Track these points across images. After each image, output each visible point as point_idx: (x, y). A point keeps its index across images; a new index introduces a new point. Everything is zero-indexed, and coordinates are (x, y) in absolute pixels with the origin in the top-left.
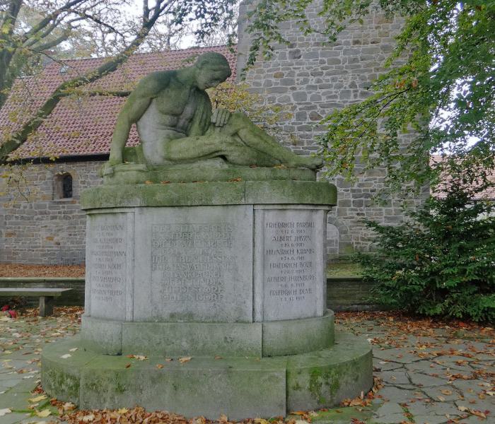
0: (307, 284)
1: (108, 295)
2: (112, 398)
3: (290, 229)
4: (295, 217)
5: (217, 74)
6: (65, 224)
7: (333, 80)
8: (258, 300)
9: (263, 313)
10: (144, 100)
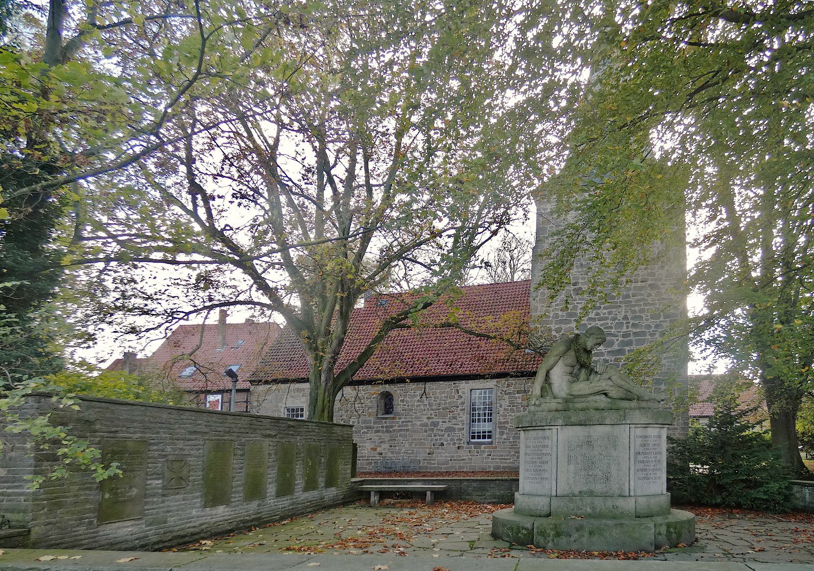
1: (539, 480)
2: (553, 540)
5: (599, 341)
6: (386, 437)
7: (609, 313)
8: (632, 483)
9: (635, 490)
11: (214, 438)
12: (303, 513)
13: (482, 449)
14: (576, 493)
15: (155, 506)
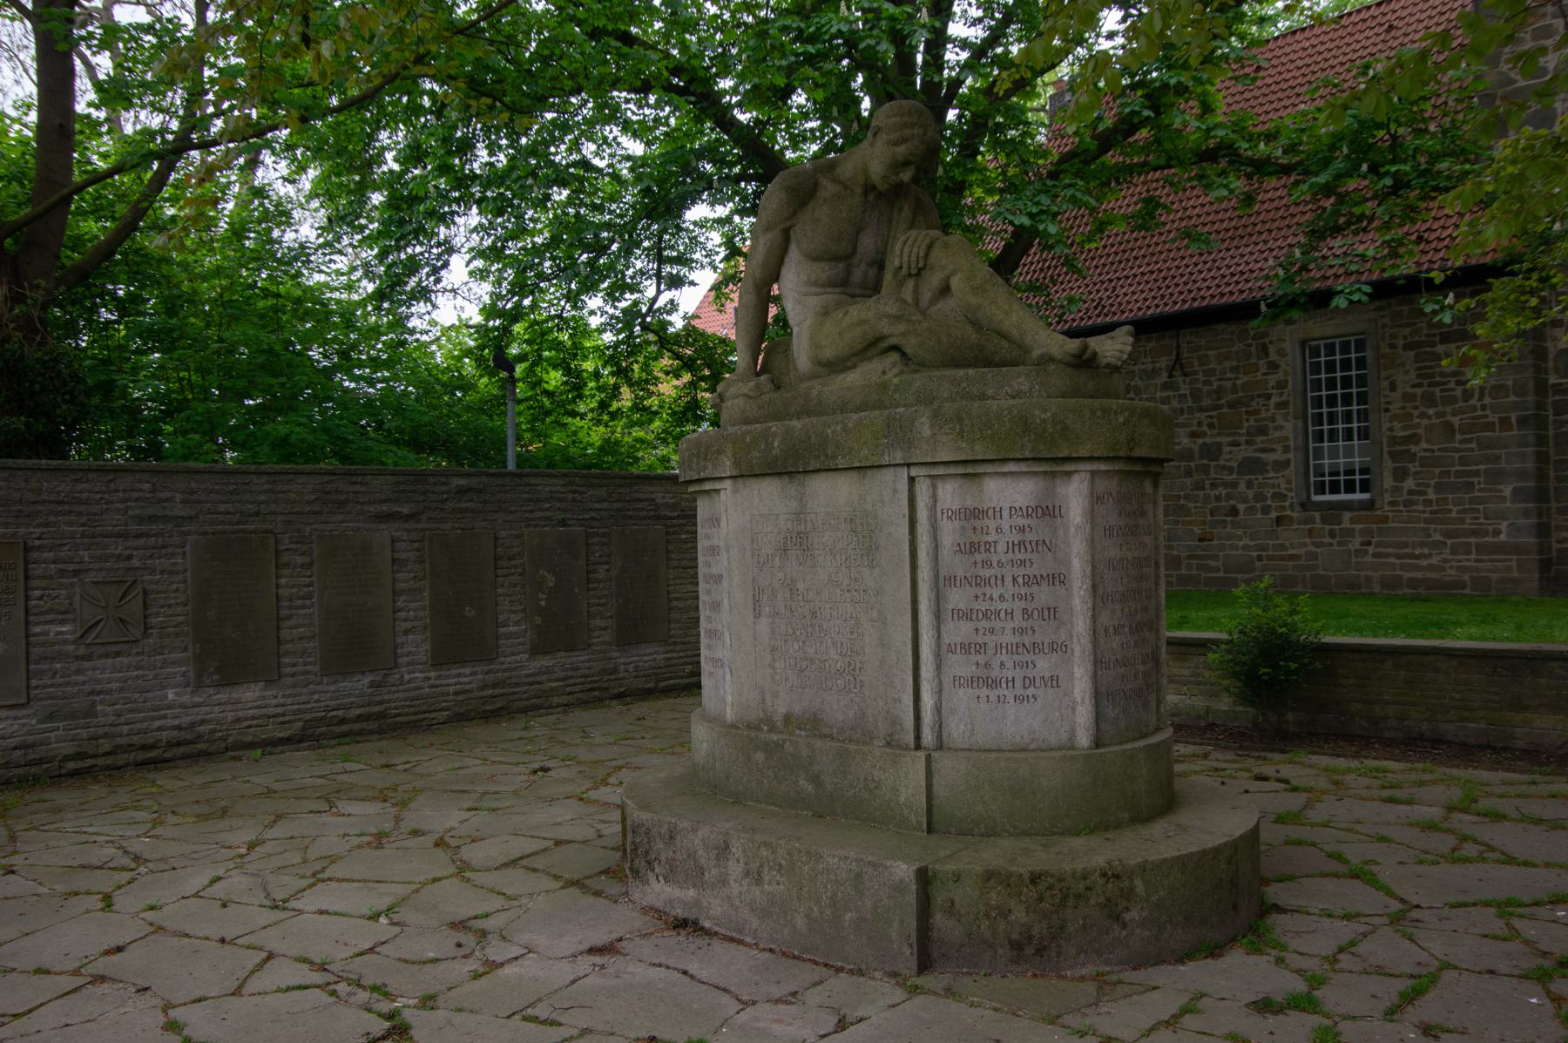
0: (1044, 665)
3: (992, 525)
4: (1009, 493)
9: (939, 726)
10: (769, 235)
11: (210, 529)
12: (536, 708)
13: (1346, 524)
14: (778, 719)
15: (58, 680)
